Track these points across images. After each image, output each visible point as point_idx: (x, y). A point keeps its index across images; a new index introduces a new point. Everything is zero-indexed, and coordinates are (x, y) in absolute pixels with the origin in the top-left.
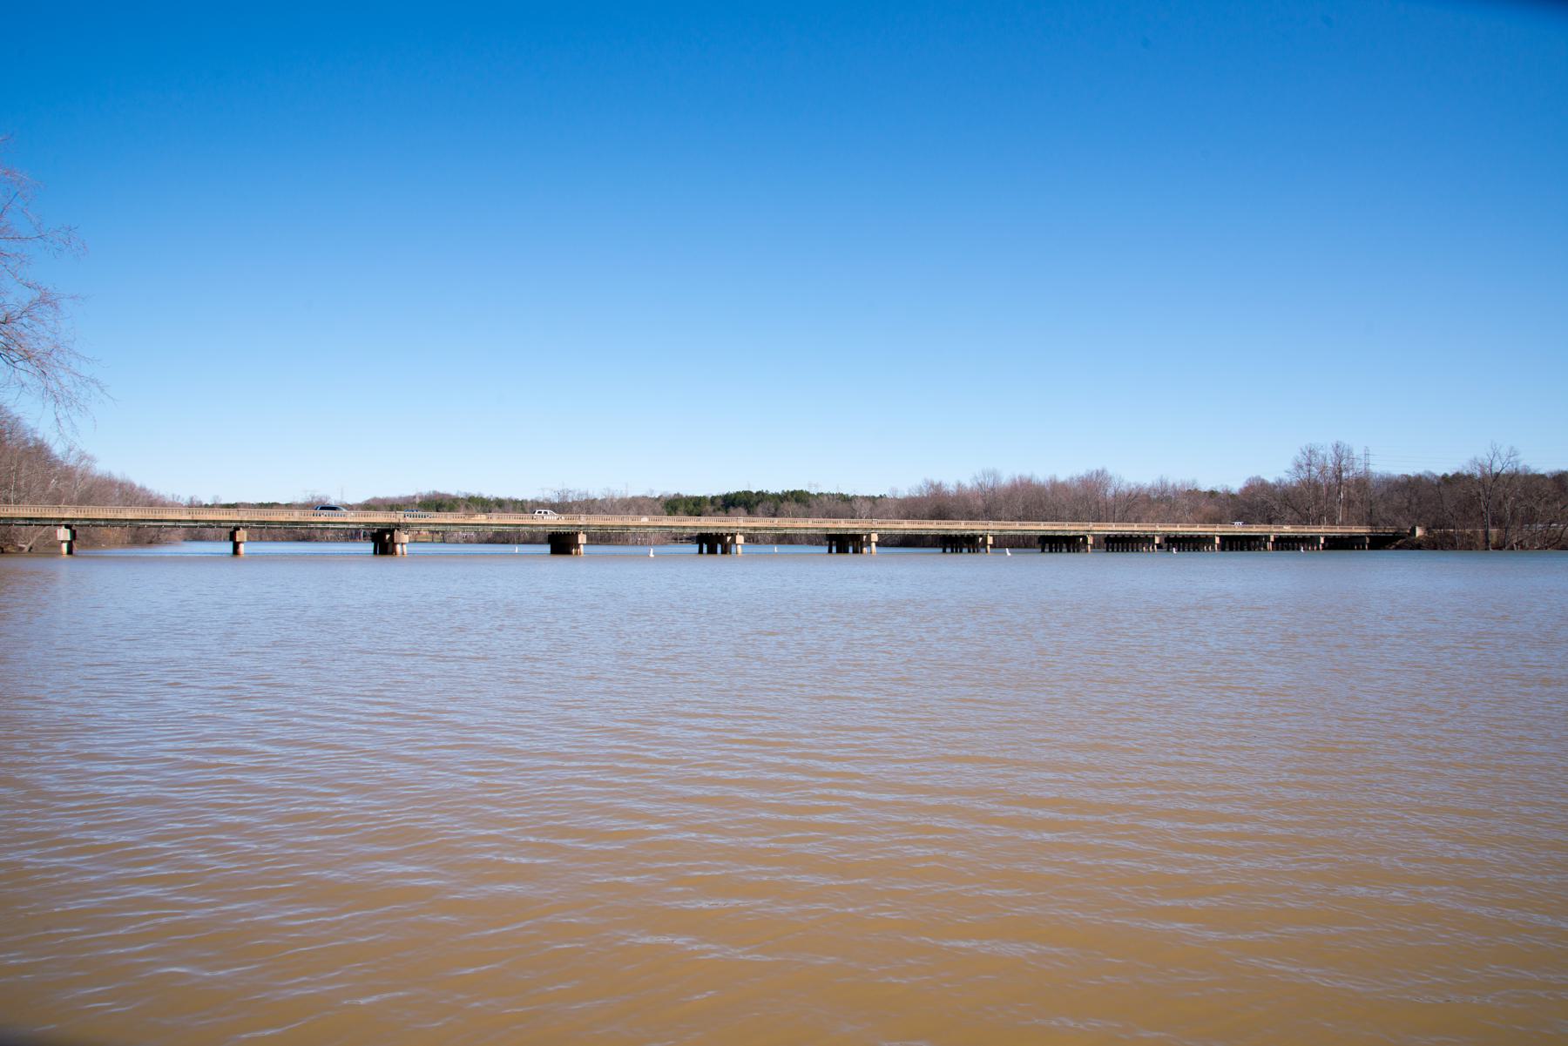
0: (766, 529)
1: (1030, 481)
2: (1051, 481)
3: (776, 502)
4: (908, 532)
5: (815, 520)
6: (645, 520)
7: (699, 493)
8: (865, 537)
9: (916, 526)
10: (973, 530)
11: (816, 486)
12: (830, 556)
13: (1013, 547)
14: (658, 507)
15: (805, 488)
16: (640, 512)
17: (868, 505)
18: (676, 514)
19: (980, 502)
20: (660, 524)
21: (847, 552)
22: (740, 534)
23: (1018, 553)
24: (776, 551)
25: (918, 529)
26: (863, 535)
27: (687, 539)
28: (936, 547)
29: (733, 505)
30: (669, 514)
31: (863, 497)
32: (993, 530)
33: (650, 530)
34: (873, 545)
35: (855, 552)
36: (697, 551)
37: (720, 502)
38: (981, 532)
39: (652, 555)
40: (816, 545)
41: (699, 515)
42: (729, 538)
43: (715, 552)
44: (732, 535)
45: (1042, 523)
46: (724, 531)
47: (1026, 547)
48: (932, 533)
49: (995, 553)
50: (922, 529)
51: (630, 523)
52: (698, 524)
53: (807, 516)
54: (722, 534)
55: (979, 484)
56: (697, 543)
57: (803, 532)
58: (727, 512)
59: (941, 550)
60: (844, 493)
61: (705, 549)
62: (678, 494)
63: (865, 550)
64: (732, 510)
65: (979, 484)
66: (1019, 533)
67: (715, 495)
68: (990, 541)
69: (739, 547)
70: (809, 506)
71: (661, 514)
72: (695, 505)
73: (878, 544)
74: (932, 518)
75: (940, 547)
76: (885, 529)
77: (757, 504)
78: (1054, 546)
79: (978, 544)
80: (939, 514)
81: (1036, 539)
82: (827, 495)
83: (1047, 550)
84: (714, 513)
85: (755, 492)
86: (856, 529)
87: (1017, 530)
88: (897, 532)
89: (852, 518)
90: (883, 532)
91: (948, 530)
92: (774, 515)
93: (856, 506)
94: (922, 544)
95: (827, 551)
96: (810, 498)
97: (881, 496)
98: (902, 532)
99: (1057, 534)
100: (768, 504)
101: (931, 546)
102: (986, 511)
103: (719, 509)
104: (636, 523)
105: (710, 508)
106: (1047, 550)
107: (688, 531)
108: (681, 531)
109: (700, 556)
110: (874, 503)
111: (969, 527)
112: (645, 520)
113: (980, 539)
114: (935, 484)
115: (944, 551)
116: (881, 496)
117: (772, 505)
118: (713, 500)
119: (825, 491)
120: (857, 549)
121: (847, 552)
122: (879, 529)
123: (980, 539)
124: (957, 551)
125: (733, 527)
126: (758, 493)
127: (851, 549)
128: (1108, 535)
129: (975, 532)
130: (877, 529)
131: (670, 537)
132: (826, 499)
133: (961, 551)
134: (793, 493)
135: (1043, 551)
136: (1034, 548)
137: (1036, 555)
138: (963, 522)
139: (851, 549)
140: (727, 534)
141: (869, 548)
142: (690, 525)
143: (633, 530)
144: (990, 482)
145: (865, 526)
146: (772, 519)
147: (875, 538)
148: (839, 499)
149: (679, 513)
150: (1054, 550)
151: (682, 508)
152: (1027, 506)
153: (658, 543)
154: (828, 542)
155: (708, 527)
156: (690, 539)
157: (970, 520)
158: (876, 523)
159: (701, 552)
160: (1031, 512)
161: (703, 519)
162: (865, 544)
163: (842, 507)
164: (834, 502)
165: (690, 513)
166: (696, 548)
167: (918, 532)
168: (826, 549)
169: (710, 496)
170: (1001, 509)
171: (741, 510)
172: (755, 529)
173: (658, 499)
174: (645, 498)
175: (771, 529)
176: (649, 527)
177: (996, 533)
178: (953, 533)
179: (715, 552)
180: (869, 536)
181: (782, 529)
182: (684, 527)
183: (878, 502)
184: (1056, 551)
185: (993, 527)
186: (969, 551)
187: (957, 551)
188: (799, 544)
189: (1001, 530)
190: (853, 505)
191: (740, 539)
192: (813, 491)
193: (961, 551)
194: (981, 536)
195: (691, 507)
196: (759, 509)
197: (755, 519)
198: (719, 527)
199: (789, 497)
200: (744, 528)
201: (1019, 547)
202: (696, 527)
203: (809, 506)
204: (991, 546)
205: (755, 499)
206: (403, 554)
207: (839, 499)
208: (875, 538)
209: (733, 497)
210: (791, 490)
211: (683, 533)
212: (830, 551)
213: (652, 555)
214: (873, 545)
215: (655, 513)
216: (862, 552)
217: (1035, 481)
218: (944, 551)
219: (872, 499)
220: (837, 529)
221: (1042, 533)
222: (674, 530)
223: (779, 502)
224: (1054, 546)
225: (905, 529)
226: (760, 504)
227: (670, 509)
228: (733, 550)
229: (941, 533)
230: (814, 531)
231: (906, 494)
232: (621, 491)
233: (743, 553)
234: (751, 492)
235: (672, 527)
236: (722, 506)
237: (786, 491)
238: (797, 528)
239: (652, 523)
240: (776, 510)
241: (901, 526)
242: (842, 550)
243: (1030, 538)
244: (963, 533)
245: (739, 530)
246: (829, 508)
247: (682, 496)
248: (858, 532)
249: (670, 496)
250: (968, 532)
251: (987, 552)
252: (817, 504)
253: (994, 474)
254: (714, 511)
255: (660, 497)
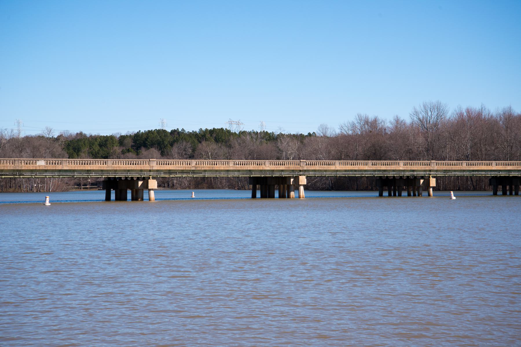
0: (182, 172)
1: (479, 114)
2: (504, 113)
3: (194, 142)
4: (339, 174)
5: (237, 161)
6: (41, 164)
7: (105, 132)
8: (292, 180)
9: (349, 167)
10: (413, 171)
11: (238, 123)
12: (254, 201)
13: (459, 190)
14: (58, 148)
15: (225, 126)
16: (36, 155)
17: (295, 145)
18: (78, 156)
19: (421, 140)
20: (59, 167)
21: (273, 196)
22: (154, 178)
23: (465, 196)
24: (194, 196)
25: (351, 171)
26: (290, 178)
27: (92, 184)
28: (372, 190)
29: (146, 146)
30: (71, 156)
31: (290, 136)
32: (437, 171)
33: (49, 175)
34: (302, 188)
35: (282, 196)
36: (104, 198)
37: (129, 143)
38: (422, 174)
39: (48, 204)
40: (239, 189)
41: (106, 157)
42: (140, 183)
43: (125, 199)
44: (144, 179)
45: (494, 162)
46: (135, 176)
47: (475, 189)
48: (368, 174)
49: (440, 196)
50: (355, 171)
51: (23, 166)
52: (104, 167)
53: (229, 157)
54: (132, 178)
55: (419, 119)
56: (103, 189)
57: (223, 175)
58: (137, 154)
59: (377, 194)
60: (269, 131)
61: (113, 196)
62: (81, 133)
63: (292, 194)
64: (143, 151)
65: (419, 119)
66: (466, 174)
67: (124, 133)
68: (433, 182)
69: (152, 192)
70: (230, 147)
71: (62, 156)
72: (101, 146)
73: (306, 188)
74: (367, 157)
75: (376, 190)
76: (315, 171)
77: (172, 145)
78: (508, 188)
79: (419, 186)
80: (375, 154)
81: (487, 181)
82: (250, 133)
83: (500, 193)
84: (123, 155)
85: (169, 130)
86: (282, 171)
87: (464, 171)
88: (328, 174)
89: (278, 158)
90: (311, 174)
91: (385, 171)
92: (192, 157)
93: (283, 145)
94: (356, 187)
95: (250, 195)
96: (232, 138)
97: (309, 134)
98: (333, 174)
99: (513, 174)
100: (184, 143)
101: (366, 189)
102: (427, 150)
103: (128, 151)
104: (31, 167)
105: (118, 149)
106: (500, 193)
107: (93, 175)
108: (85, 175)
109: (108, 203)
110: (302, 142)
111: (409, 167)
112: (41, 164)
113: (422, 181)
114: (370, 120)
115: (381, 195)
116: (309, 134)
117: (189, 145)
118: (122, 139)
119: (248, 129)
120: (284, 192)
121: (273, 196)
122: (308, 171)
123: (422, 181)
124: (395, 195)
125: (145, 170)
126: (173, 132)
127: (277, 194)
128: (493, 176)
129: (415, 173)
130: (305, 171)
131: (72, 182)
132: (248, 138)
133: (400, 195)
134: (212, 132)
135: (495, 194)
136: (485, 190)
137: (489, 198)
138: (402, 163)
139: (277, 194)
140: (138, 179)
141: (297, 192)
142: (95, 169)
143: (27, 175)
144: (433, 117)
145: (292, 167)
146: (189, 161)
147: (303, 180)
148: (262, 138)
149: (82, 154)
150: (508, 193)
151: (86, 149)
152: (475, 144)
153: (57, 190)
154: (251, 186)
155: (115, 171)
156: (96, 185)
157: (410, 159)
158: (304, 165)
159: (108, 198)
160: (481, 150)
161: (110, 161)
162: (292, 187)
163: (270, 146)
164: (259, 141)
165: (95, 156)
166: (102, 195)
167: (351, 174)
168: (249, 194)
169: (118, 136)
170: (445, 147)
171: (154, 151)
172: (170, 172)
173: (57, 139)
174: (41, 138)
175: (187, 172)
176: (46, 171)
177: (440, 174)
178: (391, 174)
179: (125, 199)
180: (297, 179)
181: (200, 172)
182: (88, 171)
183: (306, 141)
184: (511, 194)
185: (436, 168)
186: (409, 195)
187: (395, 195)
188: (219, 188)
189: (445, 171)
190: (279, 144)
191: (153, 184)
192: (235, 129)
193: (400, 195)
194: (422, 177)
195: (97, 148)
196: (175, 150)
197: (170, 161)
198: (129, 171)
199: (208, 136)
200: (157, 171)
201: (467, 189)
202: (102, 171)
203: (230, 147)
204: (433, 188)
205: (170, 139)
206: (150, 199)
207: (262, 138)
208: (303, 180)
209: (145, 136)
210: (210, 128)
211: (88, 178)
212: (254, 196)
213: (48, 204)
214: (302, 188)
215: (53, 156)
216: (289, 197)
217: (485, 114)
218: (381, 195)
219: (300, 138)
220: (261, 171)
221: (493, 174)
222: (76, 175)
223: (196, 141)
224: (508, 188)
225: (337, 171)
226: (176, 145)
227: (71, 151)
228: (145, 196)
229: (377, 174)
230: (236, 174)
231: (338, 131)
232: (12, 131)
233: (305, 197)
234: (164, 131)
235: (74, 171)
236: (132, 146)
237: (204, 129)
238: (216, 171)
239: (50, 167)
240: (194, 150)
241: (332, 168)
242: (267, 194)
243: (480, 179)
244: (402, 174)
245: (151, 173)
246: (252, 148)
247: (85, 135)
248: (284, 175)
249: (71, 135)
250: (408, 174)
251: (429, 195)
252: (240, 144)
253: (438, 108)
254: (123, 152)
255: (59, 137)
